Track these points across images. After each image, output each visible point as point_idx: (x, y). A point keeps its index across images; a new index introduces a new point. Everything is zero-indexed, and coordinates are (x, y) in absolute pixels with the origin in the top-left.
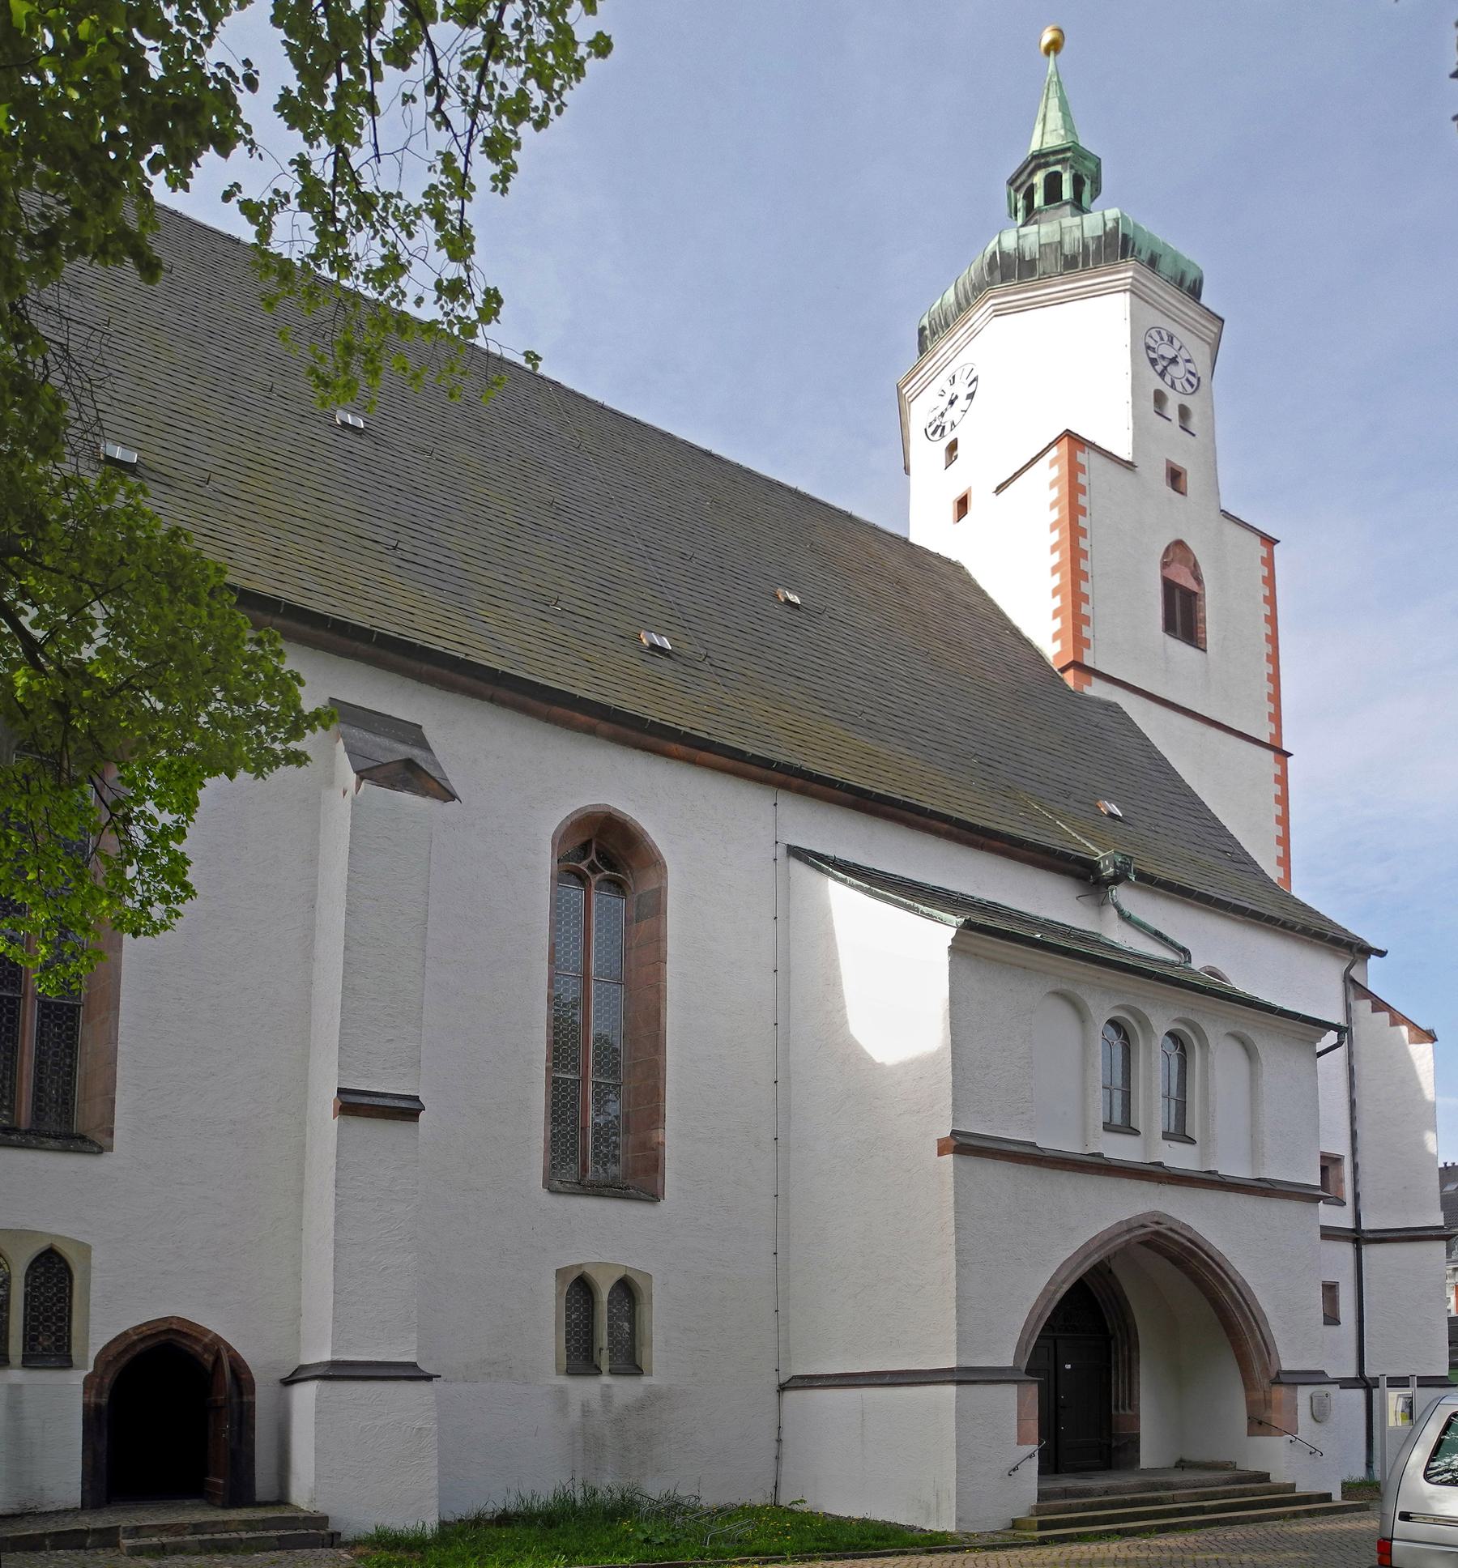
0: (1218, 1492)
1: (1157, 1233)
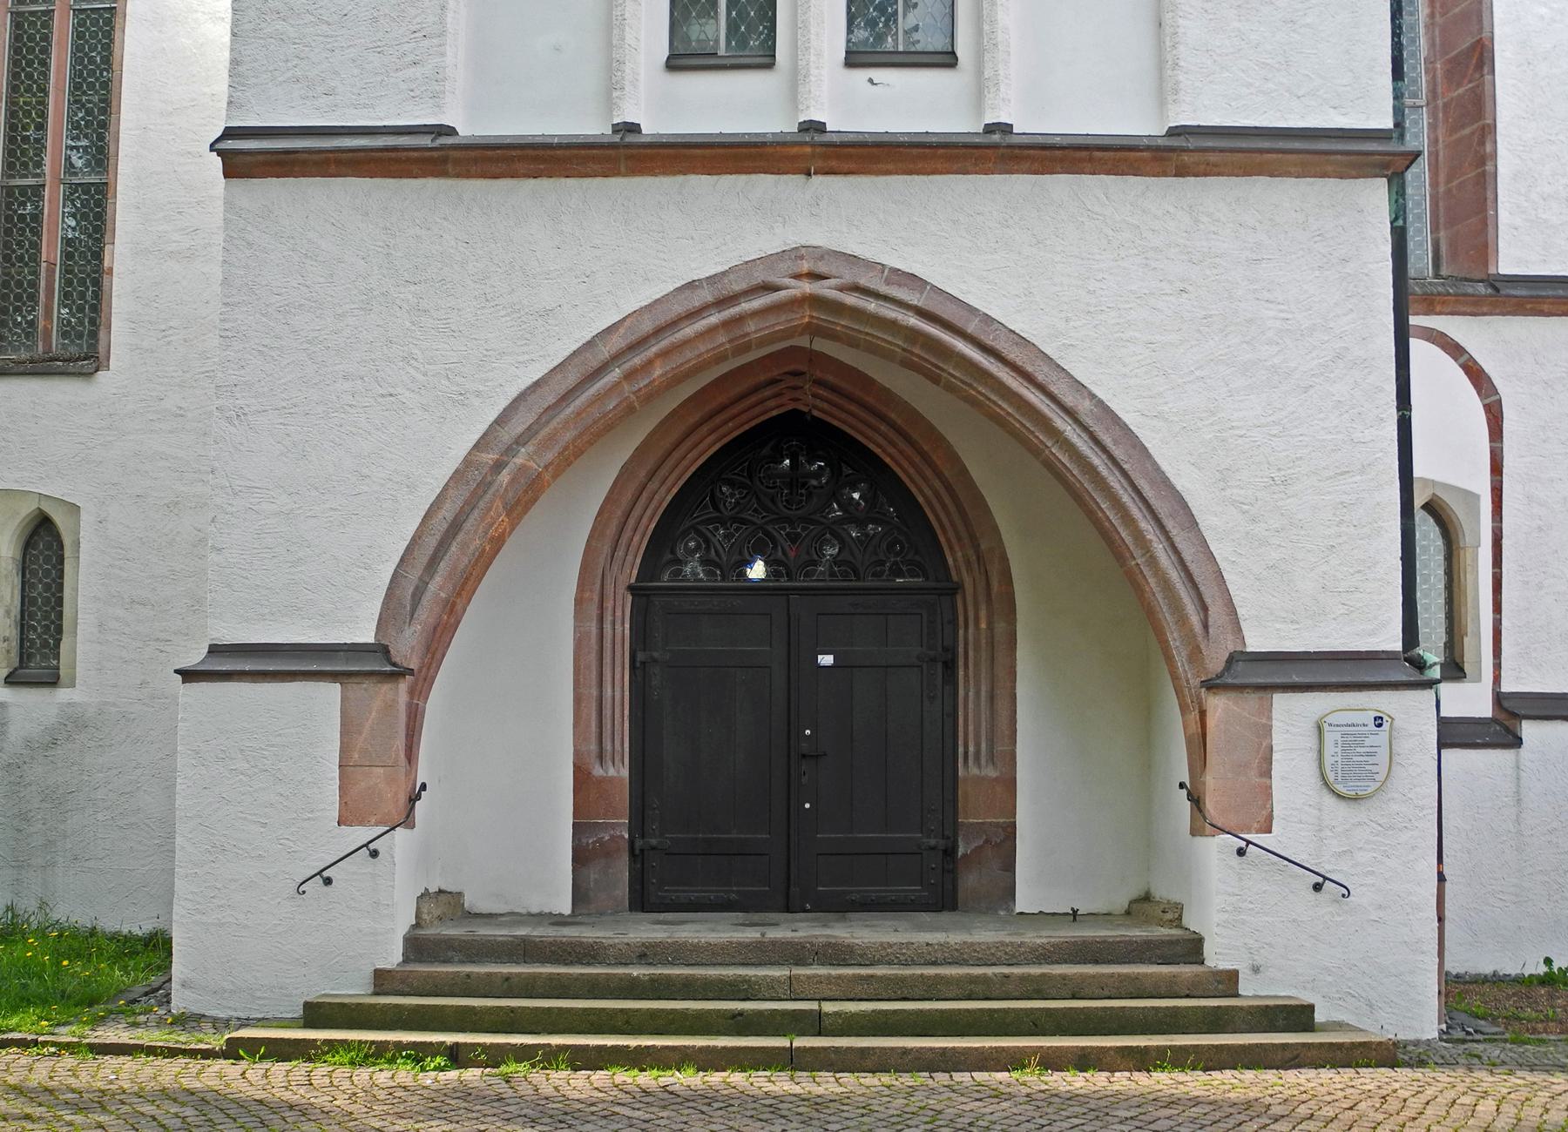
0: (985, 980)
1: (816, 301)
